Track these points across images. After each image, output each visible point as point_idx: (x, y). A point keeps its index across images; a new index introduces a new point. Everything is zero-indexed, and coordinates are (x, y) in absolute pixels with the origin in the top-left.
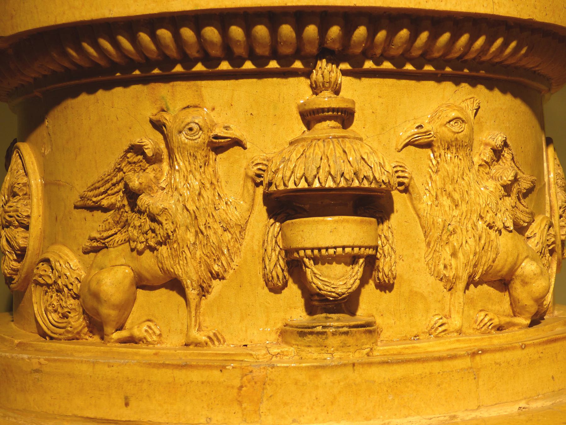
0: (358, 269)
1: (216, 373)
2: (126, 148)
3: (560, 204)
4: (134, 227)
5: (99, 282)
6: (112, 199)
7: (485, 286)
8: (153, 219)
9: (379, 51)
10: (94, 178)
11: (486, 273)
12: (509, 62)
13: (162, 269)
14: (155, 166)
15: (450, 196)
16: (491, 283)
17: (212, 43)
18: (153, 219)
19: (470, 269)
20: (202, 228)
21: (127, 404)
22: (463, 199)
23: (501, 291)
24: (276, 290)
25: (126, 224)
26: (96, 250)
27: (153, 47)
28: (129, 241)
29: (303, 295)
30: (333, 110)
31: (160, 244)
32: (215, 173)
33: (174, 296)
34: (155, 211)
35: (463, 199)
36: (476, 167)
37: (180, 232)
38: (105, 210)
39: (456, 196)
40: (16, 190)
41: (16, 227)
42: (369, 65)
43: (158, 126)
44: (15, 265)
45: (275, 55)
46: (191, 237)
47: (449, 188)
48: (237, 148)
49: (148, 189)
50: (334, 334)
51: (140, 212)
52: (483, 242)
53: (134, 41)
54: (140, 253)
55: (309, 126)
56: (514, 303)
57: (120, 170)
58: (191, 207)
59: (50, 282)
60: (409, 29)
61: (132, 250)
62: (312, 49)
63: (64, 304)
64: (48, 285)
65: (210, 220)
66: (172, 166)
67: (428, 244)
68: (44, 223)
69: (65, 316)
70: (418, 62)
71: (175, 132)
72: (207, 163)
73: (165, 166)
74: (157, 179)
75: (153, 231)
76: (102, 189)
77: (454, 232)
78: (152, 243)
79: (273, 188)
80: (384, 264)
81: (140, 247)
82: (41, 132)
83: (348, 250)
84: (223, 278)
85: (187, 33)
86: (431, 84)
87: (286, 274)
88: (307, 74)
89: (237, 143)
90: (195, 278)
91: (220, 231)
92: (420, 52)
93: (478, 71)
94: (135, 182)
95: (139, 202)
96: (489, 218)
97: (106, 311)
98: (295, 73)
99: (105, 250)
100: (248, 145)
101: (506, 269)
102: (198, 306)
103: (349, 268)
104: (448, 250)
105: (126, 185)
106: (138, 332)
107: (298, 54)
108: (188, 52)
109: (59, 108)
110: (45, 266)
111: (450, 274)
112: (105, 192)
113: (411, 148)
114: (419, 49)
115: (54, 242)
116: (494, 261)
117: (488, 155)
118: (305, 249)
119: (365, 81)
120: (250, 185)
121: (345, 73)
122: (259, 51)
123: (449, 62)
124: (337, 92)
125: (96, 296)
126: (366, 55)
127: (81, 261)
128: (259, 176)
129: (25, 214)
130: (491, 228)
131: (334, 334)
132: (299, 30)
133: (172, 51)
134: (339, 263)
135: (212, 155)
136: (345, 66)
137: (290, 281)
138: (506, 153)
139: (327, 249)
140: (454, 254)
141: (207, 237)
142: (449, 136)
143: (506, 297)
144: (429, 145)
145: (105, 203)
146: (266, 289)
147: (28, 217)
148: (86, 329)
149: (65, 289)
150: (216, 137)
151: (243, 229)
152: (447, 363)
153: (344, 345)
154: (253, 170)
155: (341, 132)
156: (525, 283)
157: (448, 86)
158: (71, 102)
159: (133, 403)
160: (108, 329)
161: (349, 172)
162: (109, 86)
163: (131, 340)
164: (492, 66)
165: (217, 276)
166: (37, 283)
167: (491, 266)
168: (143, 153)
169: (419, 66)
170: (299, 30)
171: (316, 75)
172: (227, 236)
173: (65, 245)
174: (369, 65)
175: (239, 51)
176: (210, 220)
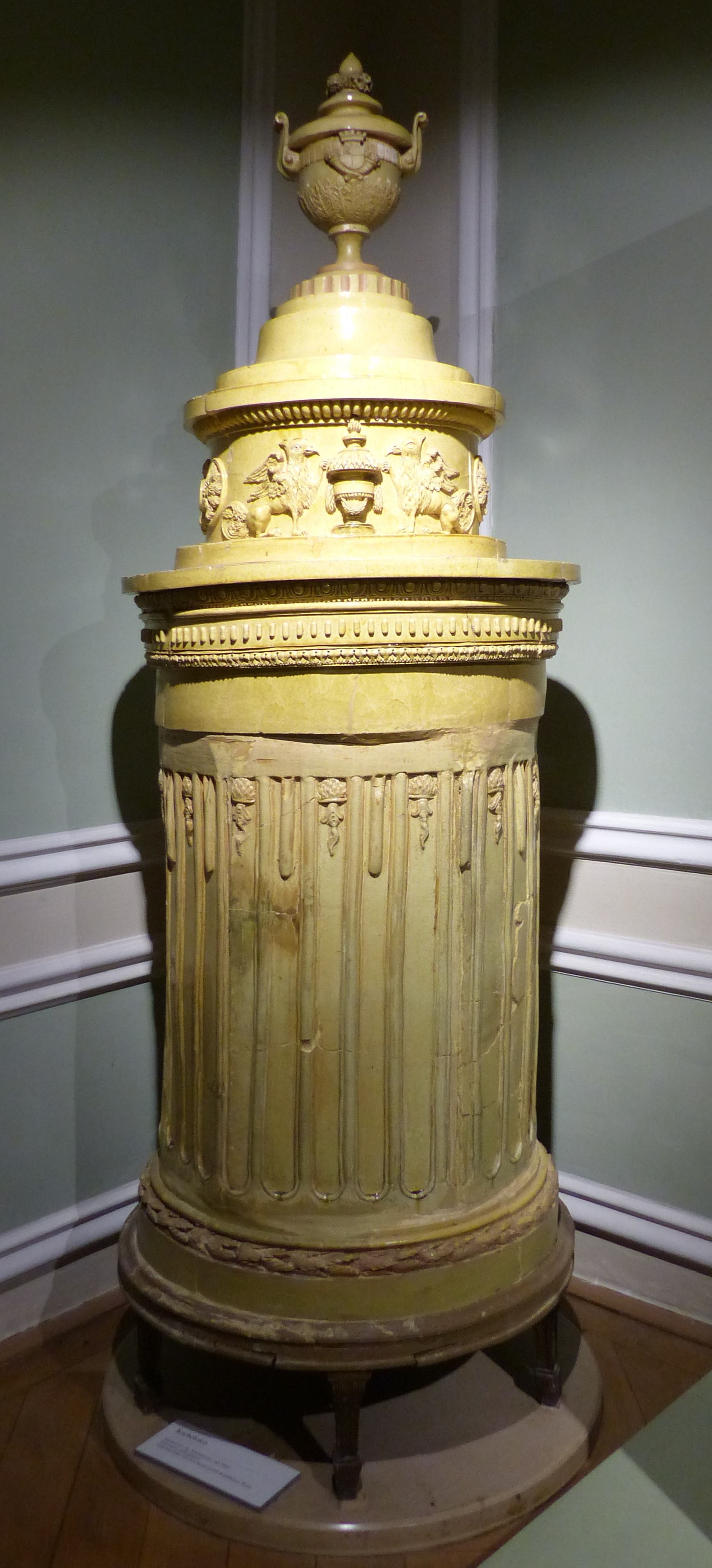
0: (365, 502)
1: (304, 540)
2: (269, 456)
3: (479, 486)
4: (271, 488)
5: (255, 511)
6: (261, 479)
7: (427, 516)
8: (279, 483)
9: (377, 415)
10: (253, 469)
11: (426, 509)
12: (440, 418)
13: (283, 505)
14: (281, 463)
15: (408, 475)
16: (431, 515)
17: (306, 413)
18: (279, 483)
19: (417, 506)
20: (300, 487)
21: (267, 555)
22: (414, 476)
23: (437, 519)
24: (330, 513)
25: (268, 487)
26: (253, 500)
27: (281, 414)
28: (268, 495)
29: (343, 515)
30: (356, 439)
31: (282, 494)
32: (306, 466)
33: (287, 517)
34: (280, 480)
35: (414, 476)
36: (422, 463)
37: (291, 489)
38: (258, 483)
39: (411, 475)
40: (214, 479)
41: (214, 495)
42: (372, 421)
43: (282, 447)
44: (212, 513)
45: (332, 417)
46: (295, 491)
47: (408, 472)
48: (316, 456)
49: (277, 472)
50: (353, 528)
51: (274, 482)
52: (423, 495)
53: (273, 412)
54: (273, 499)
55: (346, 445)
56: (442, 523)
57: (265, 465)
58: (296, 479)
59: (230, 517)
60: (389, 406)
61: (270, 498)
62: (348, 415)
63: (237, 525)
64: (230, 519)
65: (304, 484)
66: (288, 463)
67: (398, 495)
68: (229, 492)
69: (238, 531)
70: (394, 419)
71: (290, 449)
72: (302, 461)
73: (285, 463)
74: (281, 468)
75: (279, 489)
76: (257, 474)
77: (409, 491)
78: (279, 494)
79: (329, 470)
80: (377, 503)
81: (274, 496)
82: (227, 452)
83: (360, 494)
84: (308, 509)
85: (296, 409)
86: (402, 428)
87: (335, 506)
88: (346, 425)
89: (316, 453)
90: (296, 508)
91: (307, 489)
92: (395, 416)
93: (424, 423)
94: (272, 469)
95: (274, 477)
96: (426, 485)
97: (258, 523)
98: (341, 425)
99: (257, 500)
100: (320, 454)
101: (436, 508)
102: (297, 520)
103: (361, 502)
104: (407, 498)
105: (269, 471)
106: (271, 533)
107: (342, 417)
108: (296, 416)
109: (238, 441)
110: (229, 510)
111: (408, 508)
112: (258, 475)
113: (391, 455)
114: (403, 414)
115: (233, 499)
116: (429, 504)
117: (429, 458)
118: (342, 494)
119: (372, 427)
120: (321, 470)
121: (362, 424)
122: (325, 416)
123: (418, 420)
124: (359, 432)
125: (254, 517)
126: (371, 416)
127: (246, 506)
128: (325, 466)
129: (219, 489)
130: (427, 489)
131: (353, 528)
132: (342, 406)
133: (290, 416)
134: (356, 499)
135: (305, 458)
136: (363, 421)
137: (337, 510)
138: (438, 458)
139: (351, 493)
140: (410, 500)
141: (302, 491)
142: (408, 450)
143: (438, 522)
144: (399, 454)
145: (258, 480)
146: (327, 513)
147: (220, 490)
148: (248, 535)
149: (239, 519)
150: (307, 451)
151: (317, 489)
152: (398, 538)
153: (357, 532)
154: (323, 464)
155: (361, 448)
156: (445, 515)
157: (410, 429)
158: (243, 438)
159: (269, 554)
160: (258, 532)
161: (360, 463)
162: (261, 431)
163: (268, 536)
164: (436, 421)
165: (306, 508)
166: (225, 518)
167: (428, 507)
168: (276, 458)
169: (395, 421)
170: (342, 406)
171: (350, 425)
172: (310, 491)
173: (238, 500)
174: (372, 421)
175: (317, 416)
176: (304, 484)
